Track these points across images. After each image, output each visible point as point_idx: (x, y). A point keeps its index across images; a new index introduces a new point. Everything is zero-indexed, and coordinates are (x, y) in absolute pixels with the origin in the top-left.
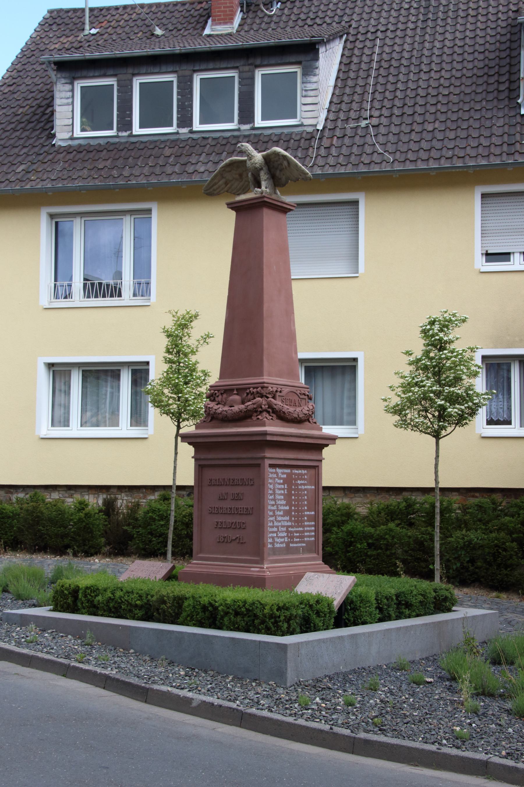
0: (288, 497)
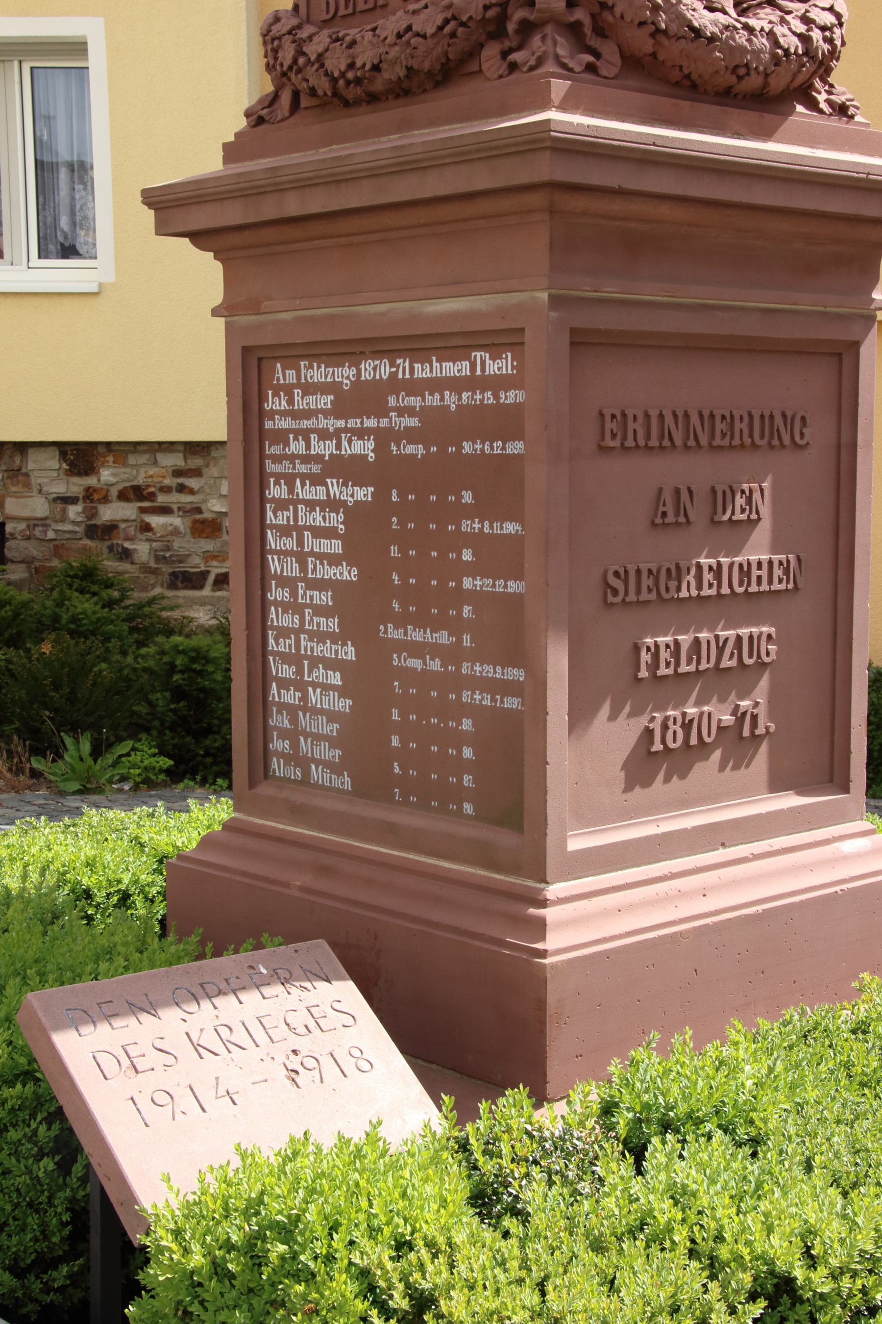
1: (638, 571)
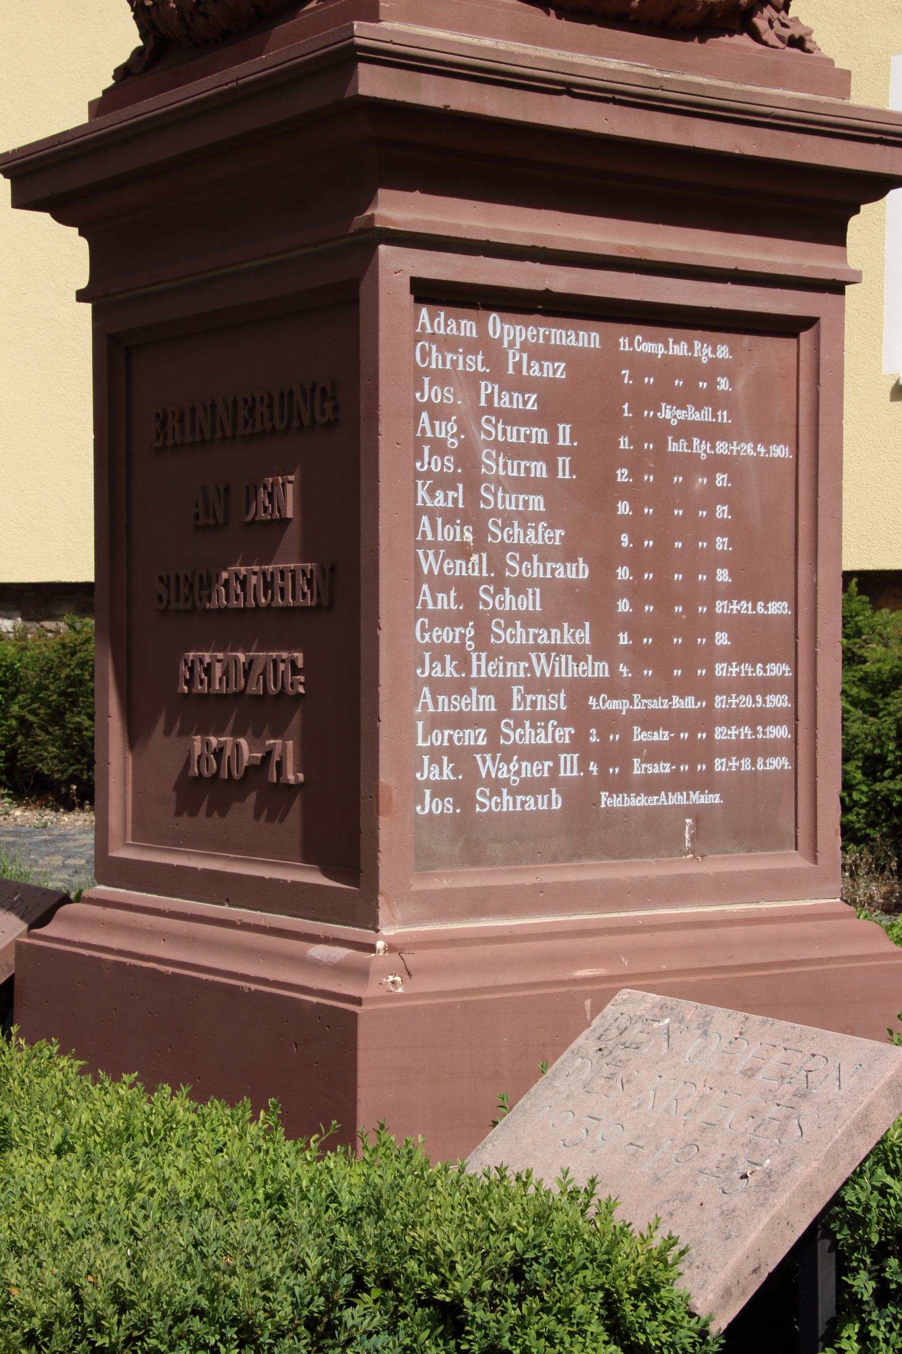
0: (583, 508)
1: (177, 577)
